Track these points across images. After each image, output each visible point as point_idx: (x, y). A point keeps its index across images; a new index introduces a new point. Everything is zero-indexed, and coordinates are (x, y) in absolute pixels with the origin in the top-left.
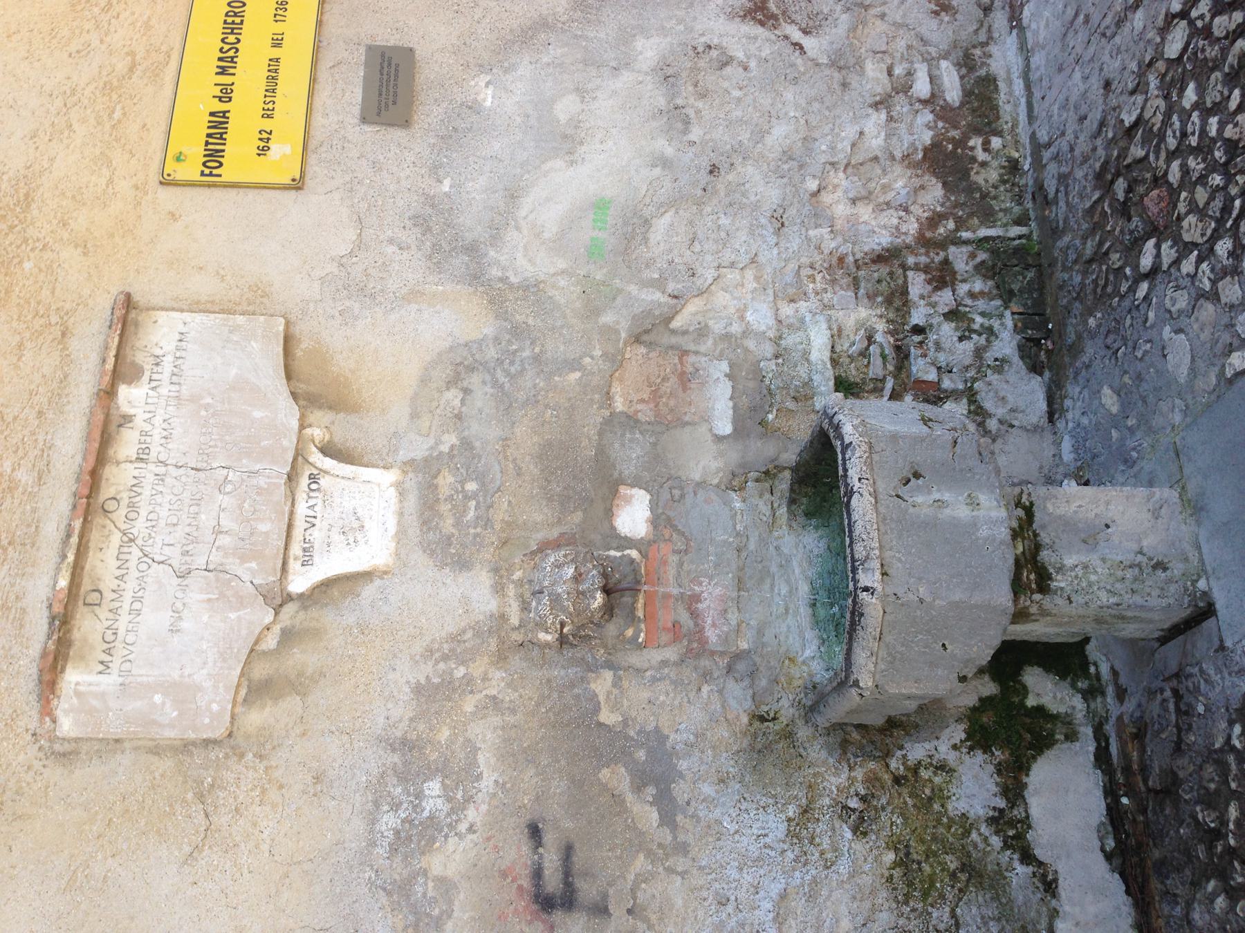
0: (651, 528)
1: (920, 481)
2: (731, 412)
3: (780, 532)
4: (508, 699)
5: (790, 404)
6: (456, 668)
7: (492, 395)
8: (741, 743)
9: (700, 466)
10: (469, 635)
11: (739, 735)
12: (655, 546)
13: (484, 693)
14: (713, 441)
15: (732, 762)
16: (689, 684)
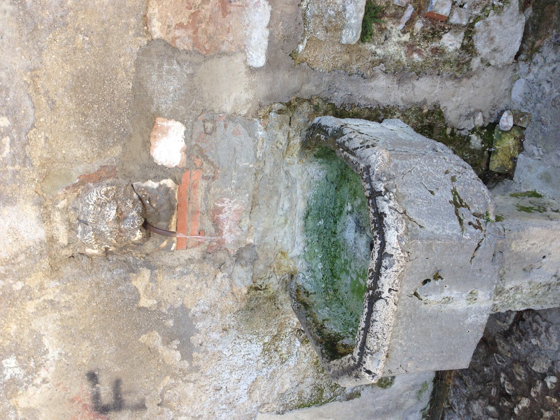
0: (185, 157)
1: (437, 283)
2: (266, 43)
3: (291, 159)
4: (63, 300)
5: (320, 34)
6: (15, 283)
7: (12, 14)
8: (241, 305)
9: (232, 98)
10: (22, 257)
11: (239, 301)
12: (188, 173)
13: (42, 299)
14: (246, 73)
15: (233, 319)
16: (208, 275)
